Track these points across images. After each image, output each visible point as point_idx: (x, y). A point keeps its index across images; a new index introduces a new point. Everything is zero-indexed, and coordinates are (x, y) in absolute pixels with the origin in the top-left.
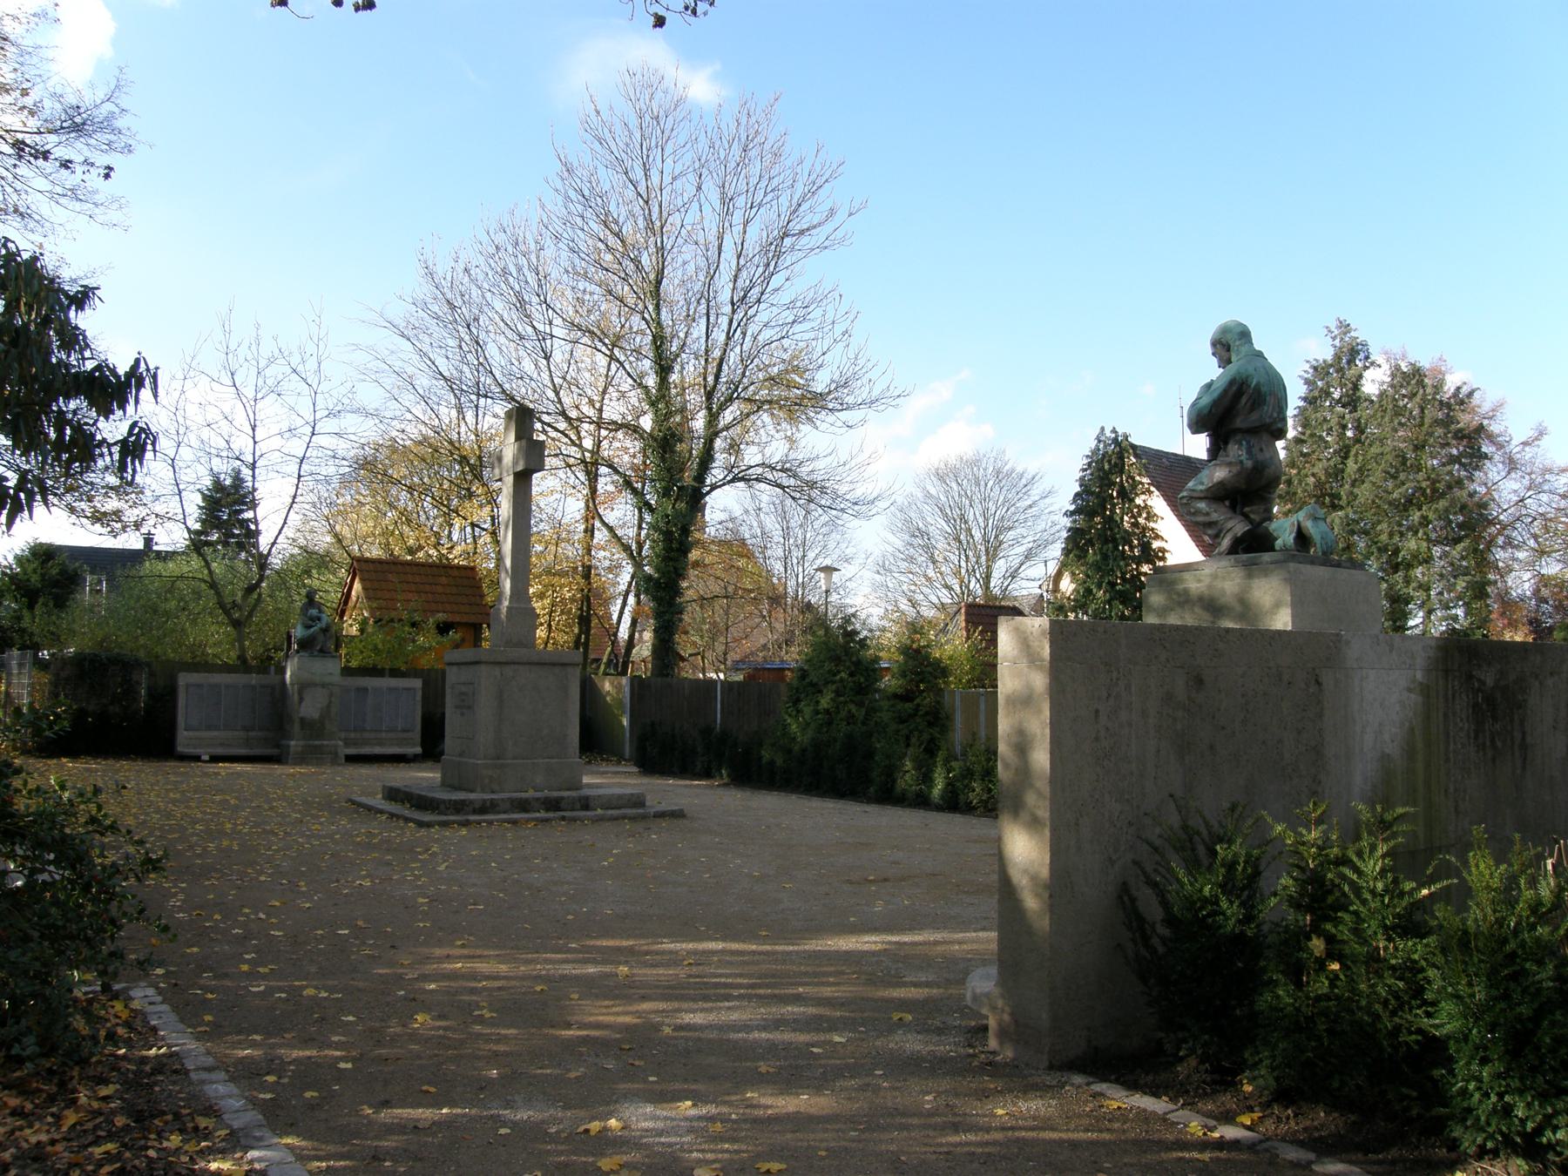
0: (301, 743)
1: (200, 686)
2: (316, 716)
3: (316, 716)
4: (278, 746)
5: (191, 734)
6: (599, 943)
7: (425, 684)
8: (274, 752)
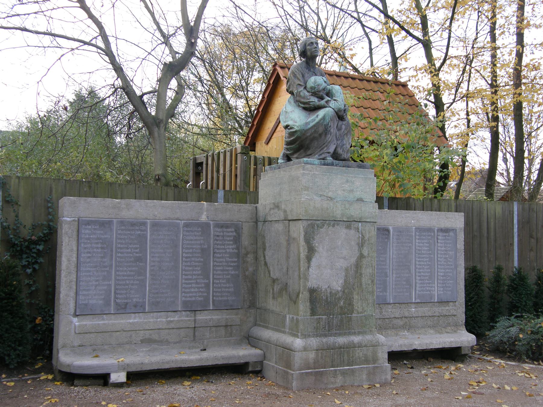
0: (314, 342)
1: (105, 224)
2: (337, 285)
3: (337, 285)
4: (250, 340)
5: (88, 322)
6: (311, 370)
7: (468, 223)
8: (242, 353)
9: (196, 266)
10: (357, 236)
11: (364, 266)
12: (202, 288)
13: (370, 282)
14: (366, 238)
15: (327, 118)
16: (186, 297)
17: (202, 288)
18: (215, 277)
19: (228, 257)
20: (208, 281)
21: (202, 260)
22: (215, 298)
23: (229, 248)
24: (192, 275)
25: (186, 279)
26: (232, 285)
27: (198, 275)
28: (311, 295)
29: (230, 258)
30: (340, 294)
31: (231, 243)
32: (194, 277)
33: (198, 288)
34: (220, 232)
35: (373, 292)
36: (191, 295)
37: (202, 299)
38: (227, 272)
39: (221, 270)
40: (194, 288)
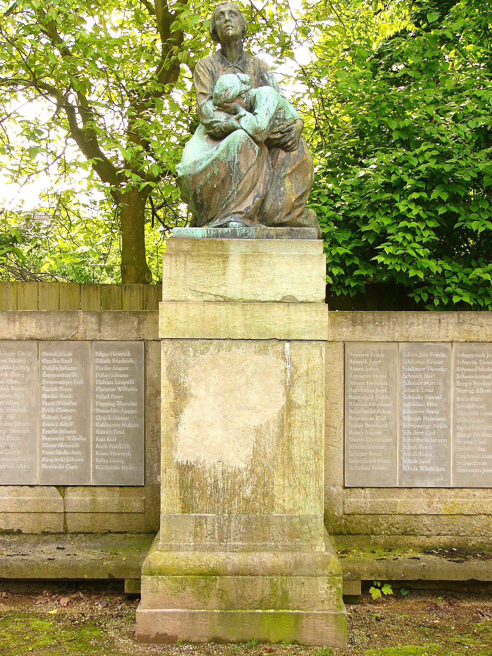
3: (238, 459)
9: (64, 414)
10: (283, 368)
11: (298, 424)
12: (75, 449)
13: (310, 454)
14: (302, 370)
15: (232, 149)
16: (48, 463)
17: (75, 449)
18: (98, 432)
19: (120, 400)
20: (85, 439)
21: (75, 404)
22: (97, 467)
23: (121, 385)
24: (58, 428)
25: (48, 436)
26: (128, 446)
27: (68, 429)
28: (182, 474)
29: (123, 401)
30: (245, 475)
31: (126, 376)
32: (62, 432)
33: (69, 449)
34: (105, 358)
35: (317, 473)
36: (56, 460)
37: (76, 467)
38: (119, 425)
39: (108, 422)
40: (62, 449)
